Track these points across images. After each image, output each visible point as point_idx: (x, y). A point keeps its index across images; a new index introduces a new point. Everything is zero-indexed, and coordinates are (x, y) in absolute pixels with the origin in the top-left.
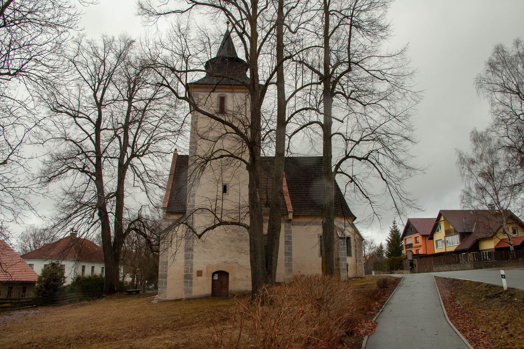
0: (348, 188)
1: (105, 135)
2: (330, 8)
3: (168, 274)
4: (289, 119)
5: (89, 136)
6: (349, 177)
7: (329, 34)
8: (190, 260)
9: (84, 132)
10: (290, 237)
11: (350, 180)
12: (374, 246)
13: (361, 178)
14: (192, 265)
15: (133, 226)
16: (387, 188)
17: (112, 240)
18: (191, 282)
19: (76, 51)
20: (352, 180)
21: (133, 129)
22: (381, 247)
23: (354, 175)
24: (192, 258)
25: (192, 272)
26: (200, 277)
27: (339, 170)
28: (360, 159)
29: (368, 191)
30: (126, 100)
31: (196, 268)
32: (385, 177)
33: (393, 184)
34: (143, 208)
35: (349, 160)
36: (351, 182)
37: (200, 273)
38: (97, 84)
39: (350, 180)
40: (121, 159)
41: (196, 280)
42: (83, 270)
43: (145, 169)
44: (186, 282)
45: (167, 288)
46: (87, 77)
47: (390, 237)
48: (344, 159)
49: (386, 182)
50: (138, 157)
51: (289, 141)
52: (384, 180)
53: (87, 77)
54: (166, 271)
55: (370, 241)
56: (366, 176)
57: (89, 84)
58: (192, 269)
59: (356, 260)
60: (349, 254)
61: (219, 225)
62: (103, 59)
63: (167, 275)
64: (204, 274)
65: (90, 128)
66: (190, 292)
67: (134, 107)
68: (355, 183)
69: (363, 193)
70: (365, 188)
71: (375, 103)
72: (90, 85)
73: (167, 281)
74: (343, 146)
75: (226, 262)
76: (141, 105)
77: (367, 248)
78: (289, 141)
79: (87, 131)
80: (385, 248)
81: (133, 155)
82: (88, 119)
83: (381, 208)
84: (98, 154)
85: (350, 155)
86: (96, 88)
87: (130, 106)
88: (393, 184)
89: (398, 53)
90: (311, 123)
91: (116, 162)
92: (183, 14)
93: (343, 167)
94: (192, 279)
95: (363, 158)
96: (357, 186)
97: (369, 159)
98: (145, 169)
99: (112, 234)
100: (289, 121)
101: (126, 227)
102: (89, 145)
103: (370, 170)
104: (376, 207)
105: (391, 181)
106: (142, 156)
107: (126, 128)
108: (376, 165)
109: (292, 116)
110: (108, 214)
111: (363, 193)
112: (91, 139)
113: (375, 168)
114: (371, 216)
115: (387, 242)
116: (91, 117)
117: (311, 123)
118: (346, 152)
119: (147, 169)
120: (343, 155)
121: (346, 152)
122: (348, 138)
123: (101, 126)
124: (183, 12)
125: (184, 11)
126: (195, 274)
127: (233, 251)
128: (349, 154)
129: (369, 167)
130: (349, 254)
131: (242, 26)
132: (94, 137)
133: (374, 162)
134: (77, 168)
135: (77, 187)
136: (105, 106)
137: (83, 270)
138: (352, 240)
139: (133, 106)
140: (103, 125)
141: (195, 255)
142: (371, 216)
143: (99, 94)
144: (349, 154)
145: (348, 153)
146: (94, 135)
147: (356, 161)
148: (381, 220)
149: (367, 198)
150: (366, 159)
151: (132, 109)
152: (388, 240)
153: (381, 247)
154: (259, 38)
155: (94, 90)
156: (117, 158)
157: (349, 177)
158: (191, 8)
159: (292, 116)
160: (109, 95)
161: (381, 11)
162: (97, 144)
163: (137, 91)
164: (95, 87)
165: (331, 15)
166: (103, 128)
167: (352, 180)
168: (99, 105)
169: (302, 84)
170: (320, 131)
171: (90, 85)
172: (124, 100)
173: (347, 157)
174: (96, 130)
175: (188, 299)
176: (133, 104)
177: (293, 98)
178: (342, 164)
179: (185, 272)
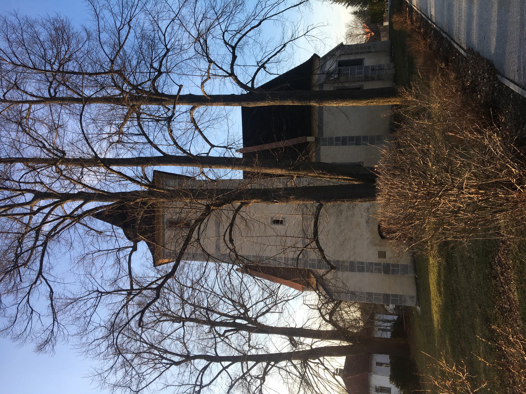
0: (274, 71)
1: (222, 351)
2: (47, 95)
3: (382, 292)
4: (184, 151)
5: (224, 368)
6: (258, 70)
7: (79, 97)
8: (365, 266)
9: (220, 376)
10: (337, 139)
11: (262, 69)
12: (353, 23)
13: (261, 54)
14: (371, 263)
15: (327, 317)
16: (272, 18)
17: (345, 344)
18: (394, 265)
19: (124, 390)
20: (263, 66)
21: (215, 317)
22: (355, 13)
23: (256, 64)
24: (362, 263)
25: (379, 264)
26: (387, 254)
27: (249, 85)
28: (234, 57)
29: (278, 44)
30: (183, 324)
31: (374, 258)
32: (257, 23)
33: (266, 10)
34: (307, 303)
35: (237, 71)
36: (265, 68)
37: (382, 255)
38: (164, 361)
39: (262, 69)
40: (250, 330)
41: (390, 259)
42: (381, 364)
43: (262, 301)
44: (394, 272)
45: (401, 294)
46: (157, 374)
47: (343, 3)
48: (236, 79)
49: (264, 20)
50: (247, 310)
51: (217, 146)
52: (260, 24)
53: (157, 374)
54: (380, 294)
55: (348, 29)
56: (258, 47)
57: (163, 372)
58: (376, 264)
59: (369, 52)
60: (360, 62)
61: (318, 243)
62: (134, 355)
63: (384, 294)
64: (383, 249)
65: (216, 367)
66: (406, 266)
67: (191, 315)
68: (266, 62)
69: (278, 52)
70: (274, 48)
71: (164, 35)
72: (165, 371)
73: (392, 295)
74: (218, 80)
75: (367, 222)
76: (188, 309)
77: (355, 32)
78: (217, 146)
79: (216, 380)
80: (356, 8)
81: (244, 316)
82: (203, 373)
83: (298, 25)
84: (243, 358)
85: (229, 72)
86: (169, 362)
87: (190, 320)
88: (266, 10)
89: (91, 6)
90: (193, 121)
91: (254, 335)
92: (54, 291)
93: (245, 79)
94: (388, 265)
95: (234, 53)
96: (270, 60)
97: (233, 45)
98: (262, 301)
99: (335, 343)
100: (188, 151)
101: (330, 327)
102: (236, 369)
103: (251, 41)
104: (297, 32)
105: (263, 13)
106: (245, 306)
107: (213, 324)
108: (243, 33)
109: (181, 149)
110: (324, 277)
111: (278, 52)
112: (227, 367)
113: (248, 35)
114: (309, 39)
115: (350, 7)
116: (200, 368)
117: (193, 121)
118: (225, 76)
119: (261, 299)
120: (229, 80)
121: (225, 76)
122: (206, 74)
123: (212, 355)
124: (52, 291)
125: (49, 290)
126: (382, 261)
127: (354, 214)
128: (227, 73)
129: (246, 43)
130: (360, 62)
131: (62, 219)
132: (226, 364)
133: (239, 36)
134: (261, 384)
135: (283, 381)
136: (188, 351)
137: (381, 364)
138: (343, 58)
139: (190, 316)
140: (211, 353)
141: (359, 260)
142: (309, 39)
143: (176, 359)
144: (227, 73)
145: (225, 74)
146: (223, 363)
147: (238, 61)
148: (314, 25)
149: (285, 45)
150: (234, 48)
151: (193, 316)
152: (346, 5)
153: (355, 13)
154: (83, 190)
155: (171, 365)
156: (249, 334)
157: (258, 70)
158: (46, 280)
159: (181, 149)
160: (177, 348)
161: (39, 28)
162: (233, 360)
163: (172, 312)
164: (167, 364)
165: (56, 93)
166: (215, 353)
167: (263, 66)
168: (188, 358)
169: (140, 134)
170: (201, 109)
171: (165, 371)
172: (183, 325)
173: (232, 74)
174: (218, 362)
175: (416, 270)
176: (188, 316)
177: (160, 147)
178: (242, 81)
179: (379, 271)
